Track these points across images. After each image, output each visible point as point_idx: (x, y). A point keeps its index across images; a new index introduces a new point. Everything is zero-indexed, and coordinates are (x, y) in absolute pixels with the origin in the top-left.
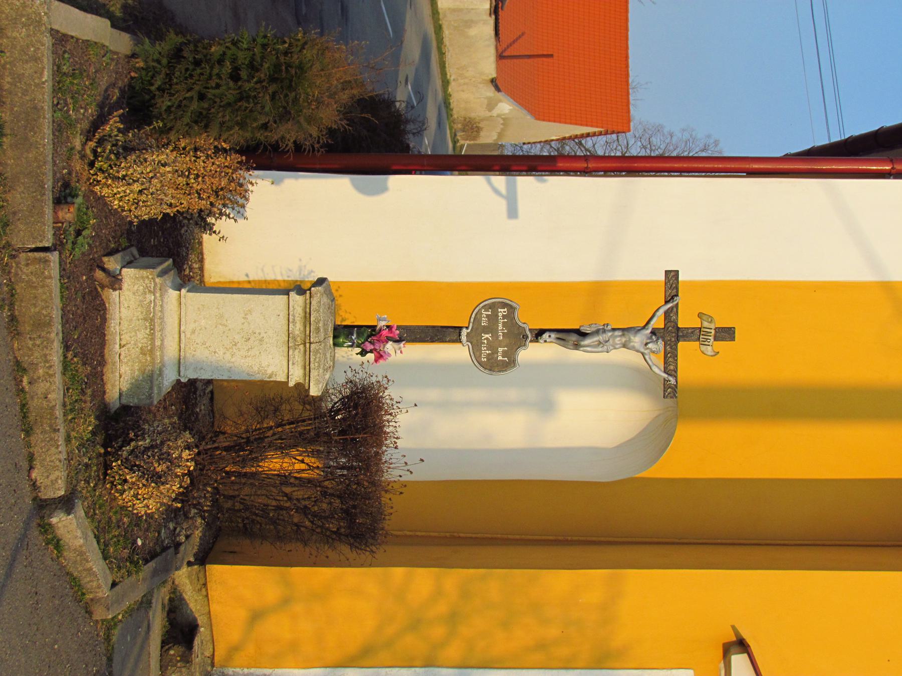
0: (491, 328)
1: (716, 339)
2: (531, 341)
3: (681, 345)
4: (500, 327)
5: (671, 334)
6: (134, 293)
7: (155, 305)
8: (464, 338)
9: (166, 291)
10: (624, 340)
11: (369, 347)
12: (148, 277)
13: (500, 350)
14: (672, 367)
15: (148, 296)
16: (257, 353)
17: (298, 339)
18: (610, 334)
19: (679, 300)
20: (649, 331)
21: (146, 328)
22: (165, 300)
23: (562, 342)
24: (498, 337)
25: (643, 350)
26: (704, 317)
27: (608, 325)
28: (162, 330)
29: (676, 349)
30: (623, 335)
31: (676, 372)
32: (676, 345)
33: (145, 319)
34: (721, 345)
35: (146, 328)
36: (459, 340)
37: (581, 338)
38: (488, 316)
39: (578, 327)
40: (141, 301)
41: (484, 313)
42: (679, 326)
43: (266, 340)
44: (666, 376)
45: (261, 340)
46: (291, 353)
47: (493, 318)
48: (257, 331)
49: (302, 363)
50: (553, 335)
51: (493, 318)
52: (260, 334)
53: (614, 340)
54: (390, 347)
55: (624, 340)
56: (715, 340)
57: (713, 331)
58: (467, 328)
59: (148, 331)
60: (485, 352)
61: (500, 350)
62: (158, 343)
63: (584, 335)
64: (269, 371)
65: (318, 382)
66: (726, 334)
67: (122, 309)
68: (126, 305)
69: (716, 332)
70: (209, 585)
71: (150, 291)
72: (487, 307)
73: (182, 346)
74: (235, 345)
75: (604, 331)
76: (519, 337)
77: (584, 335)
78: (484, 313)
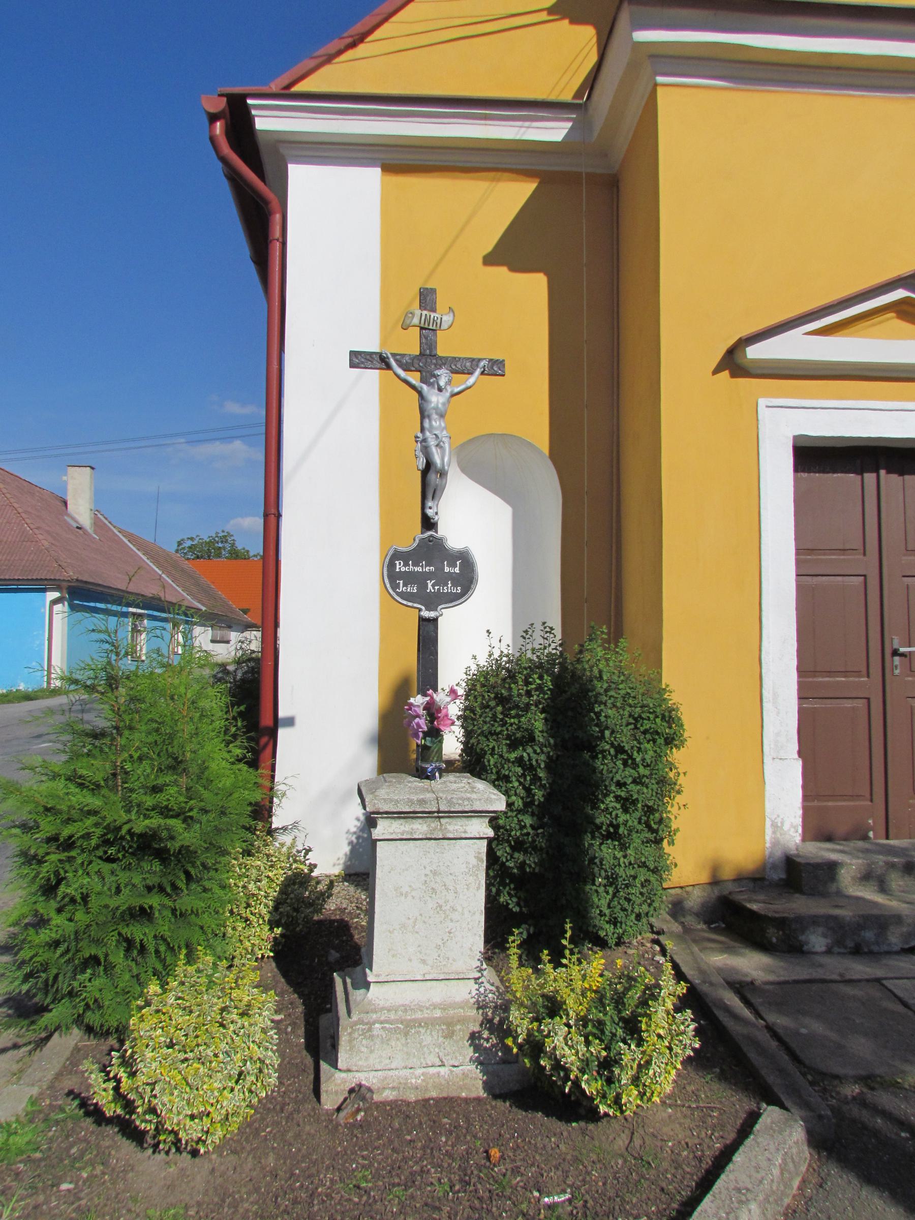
0: (420, 579)
1: (434, 310)
2: (436, 532)
3: (441, 352)
4: (419, 569)
5: (426, 362)
6: (372, 1052)
7: (386, 1022)
8: (432, 614)
9: (370, 1002)
10: (435, 416)
11: (522, 904)
12: (350, 1034)
13: (447, 569)
14: (468, 364)
15: (375, 1033)
16: (451, 877)
17: (433, 825)
18: (428, 434)
19: (387, 352)
20: (425, 387)
21: (418, 1032)
22: (382, 1003)
23: (438, 492)
24: (430, 573)
25: (448, 394)
26: (408, 322)
27: (417, 437)
28: (421, 1008)
29: (446, 358)
30: (429, 417)
31: (473, 360)
32: (441, 358)
33: (406, 1035)
34: (441, 302)
35: (418, 1032)
36: (435, 621)
37: (432, 469)
38: (405, 585)
39: (419, 474)
40: (382, 1043)
41: (401, 589)
42: (418, 353)
43: (434, 867)
44: (478, 371)
45: (435, 873)
46: (451, 836)
47: (409, 578)
48: (423, 878)
49: (464, 819)
50: (430, 503)
51: (409, 578)
52: (426, 875)
53: (436, 429)
54: (273, 826)
55: (435, 416)
56: (434, 311)
57: (424, 313)
58: (420, 610)
59: (422, 1030)
60: (449, 588)
61: (447, 569)
62: (438, 1013)
63: (429, 466)
64: (474, 861)
65: (489, 800)
66: (427, 298)
67: (393, 1066)
68: (388, 1061)
69: (425, 309)
70: (682, 885)
71: (370, 1029)
72: (395, 586)
73: (442, 977)
74: (441, 907)
75: (425, 440)
76: (431, 548)
77: (429, 466)
78: (401, 589)
